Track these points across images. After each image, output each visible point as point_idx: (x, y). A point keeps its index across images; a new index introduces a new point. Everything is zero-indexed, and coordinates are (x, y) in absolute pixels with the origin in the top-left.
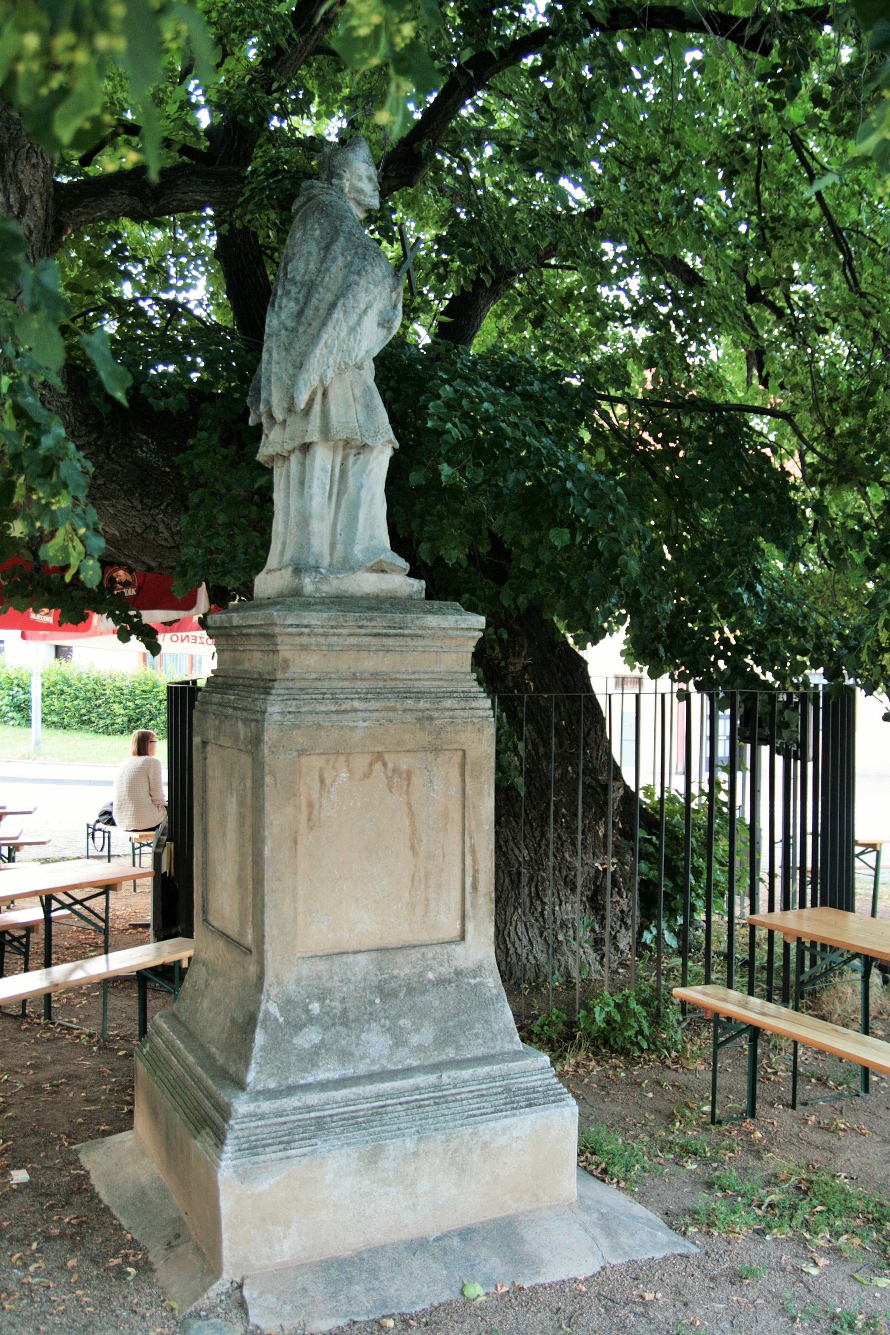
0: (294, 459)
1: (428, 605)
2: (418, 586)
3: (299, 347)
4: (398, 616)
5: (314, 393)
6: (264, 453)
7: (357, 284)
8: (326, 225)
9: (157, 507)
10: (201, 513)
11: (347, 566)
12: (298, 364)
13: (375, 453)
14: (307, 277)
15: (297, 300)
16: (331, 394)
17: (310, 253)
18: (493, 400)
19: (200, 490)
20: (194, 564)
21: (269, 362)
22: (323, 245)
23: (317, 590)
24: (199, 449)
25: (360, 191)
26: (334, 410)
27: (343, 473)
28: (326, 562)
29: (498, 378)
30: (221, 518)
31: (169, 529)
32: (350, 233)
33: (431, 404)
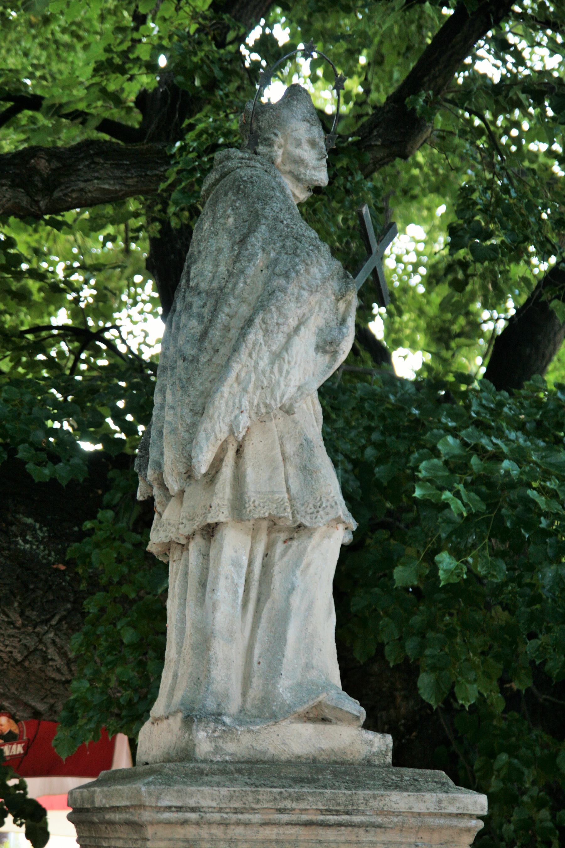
0: (194, 548)
1: (395, 773)
2: (381, 743)
3: (199, 384)
4: (342, 794)
5: (223, 449)
6: (157, 538)
7: (284, 290)
8: (243, 209)
9: (46, 622)
10: (100, 630)
11: (267, 712)
12: (198, 409)
13: (316, 537)
14: (215, 285)
15: (200, 317)
16: (249, 452)
17: (220, 250)
18: (520, 456)
19: (99, 595)
20: (86, 706)
21: (162, 407)
22: (237, 238)
23: (217, 750)
24: (100, 535)
25: (299, 161)
26: (251, 474)
27: (266, 567)
28: (233, 706)
29: (539, 424)
30: (128, 636)
31: (63, 654)
32: (276, 219)
33: (423, 465)
